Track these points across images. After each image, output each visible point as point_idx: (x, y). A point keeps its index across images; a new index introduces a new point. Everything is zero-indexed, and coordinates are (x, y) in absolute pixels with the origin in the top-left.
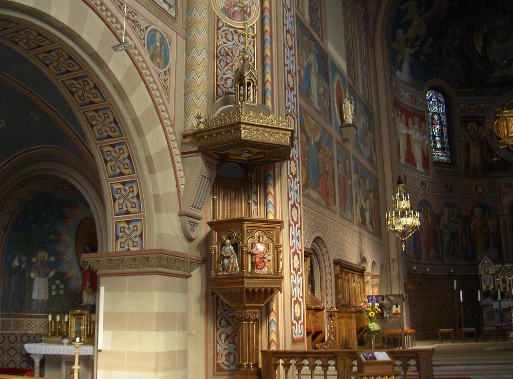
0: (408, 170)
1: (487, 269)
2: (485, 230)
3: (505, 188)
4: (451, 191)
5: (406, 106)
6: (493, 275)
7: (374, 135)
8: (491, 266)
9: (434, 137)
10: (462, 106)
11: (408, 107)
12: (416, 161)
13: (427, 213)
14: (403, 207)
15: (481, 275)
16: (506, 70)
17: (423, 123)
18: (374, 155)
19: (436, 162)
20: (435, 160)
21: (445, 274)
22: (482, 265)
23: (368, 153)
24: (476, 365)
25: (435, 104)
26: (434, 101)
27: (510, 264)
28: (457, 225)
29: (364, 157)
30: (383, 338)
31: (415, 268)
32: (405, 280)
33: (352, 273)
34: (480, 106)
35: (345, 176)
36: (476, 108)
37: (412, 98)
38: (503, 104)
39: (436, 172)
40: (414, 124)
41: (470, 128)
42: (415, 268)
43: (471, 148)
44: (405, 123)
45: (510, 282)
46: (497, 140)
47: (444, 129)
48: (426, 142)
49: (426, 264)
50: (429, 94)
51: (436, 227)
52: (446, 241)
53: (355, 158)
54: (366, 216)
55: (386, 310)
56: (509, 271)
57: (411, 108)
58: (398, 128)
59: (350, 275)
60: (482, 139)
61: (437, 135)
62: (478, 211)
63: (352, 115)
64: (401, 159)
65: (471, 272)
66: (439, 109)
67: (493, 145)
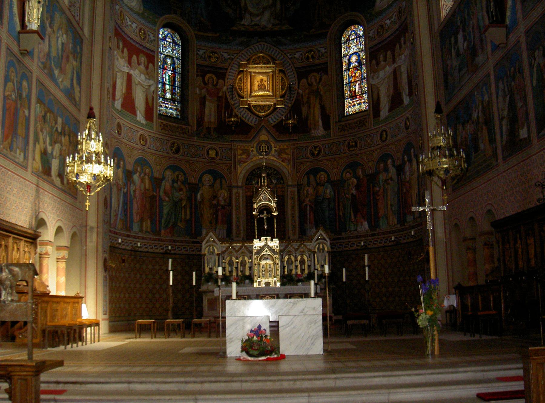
0: (124, 118)
1: (211, 248)
2: (214, 202)
3: (241, 155)
4: (177, 151)
5: (131, 39)
6: (218, 255)
7: (81, 63)
8: (217, 244)
9: (164, 84)
10: (201, 52)
11: (134, 41)
12: (136, 109)
13: (145, 174)
14: (91, 149)
15: (205, 255)
16: (258, 18)
17: (151, 65)
18: (77, 90)
19: (162, 115)
20: (161, 113)
21: (161, 251)
22: (207, 243)
23: (67, 83)
24: (141, 383)
25: (169, 45)
26: (168, 42)
27: (240, 244)
28: (181, 193)
29: (59, 87)
30: (44, 331)
31: (120, 240)
32: (105, 255)
33: (14, 238)
34: (223, 55)
35: (19, 102)
36: (217, 58)
37: (140, 31)
38: (249, 57)
39: (160, 126)
40: (139, 64)
41: (208, 81)
42: (120, 240)
43: (207, 103)
44: (127, 58)
45: (237, 265)
46: (237, 97)
47: (178, 76)
48: (152, 89)
49: (138, 238)
50: (162, 33)
51: (155, 193)
52: (165, 212)
53: (40, 83)
54: (51, 164)
55: (5, 289)
56: (237, 251)
57: (138, 43)
58: (116, 63)
59: (11, 240)
60: (221, 94)
61: (167, 83)
62: (208, 179)
63: (38, 19)
64: (116, 102)
65: (187, 251)
66: (173, 52)
67: (233, 103)
